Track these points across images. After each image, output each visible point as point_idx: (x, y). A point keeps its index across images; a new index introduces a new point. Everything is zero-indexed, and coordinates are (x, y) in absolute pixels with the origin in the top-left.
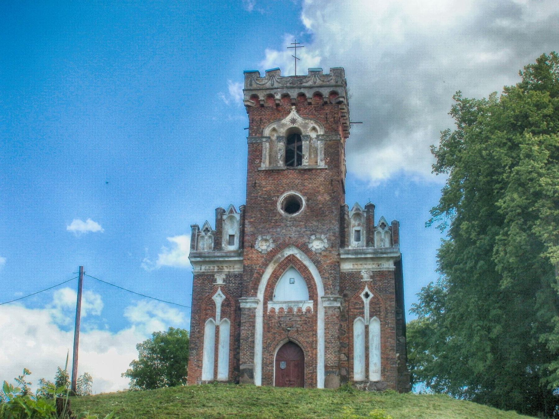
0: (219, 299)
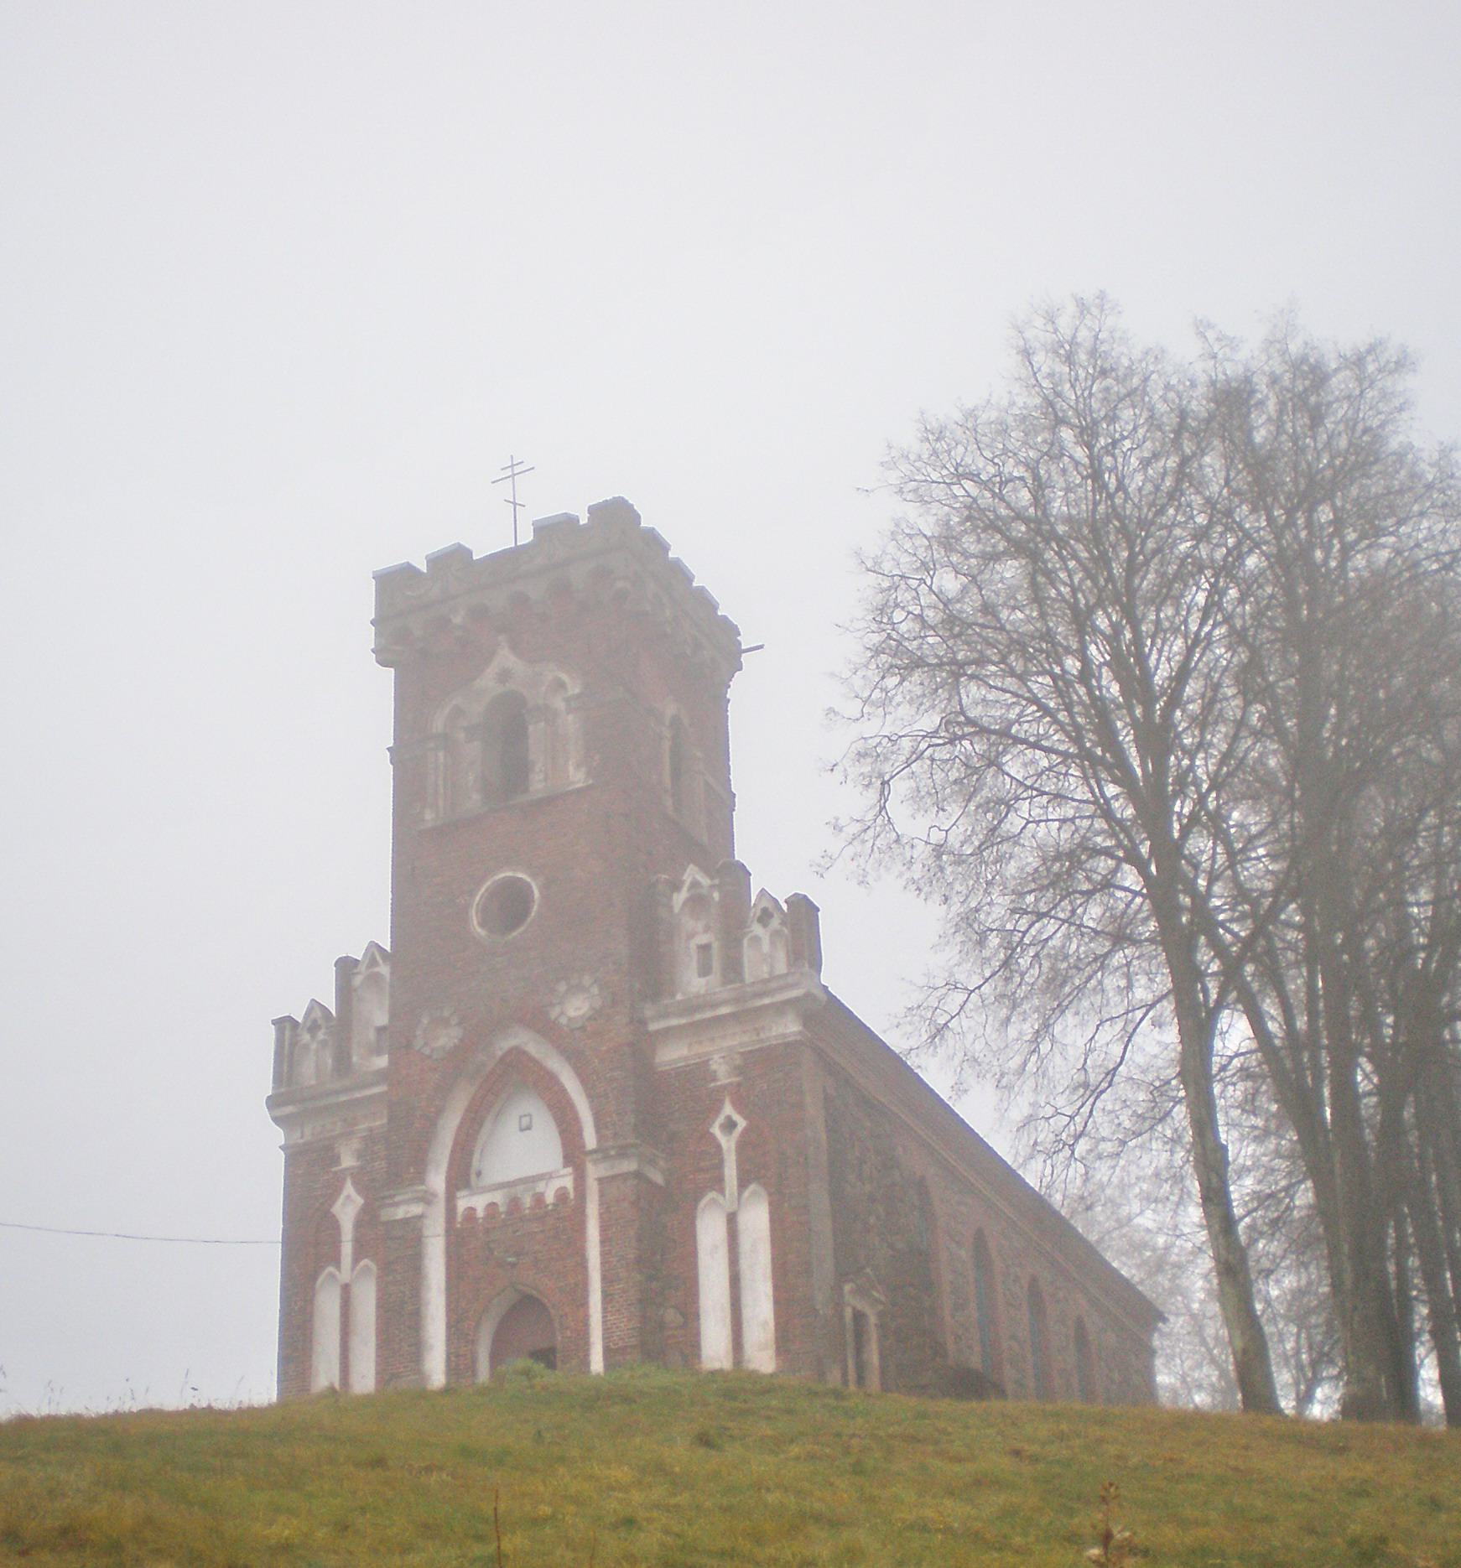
0: (348, 1208)
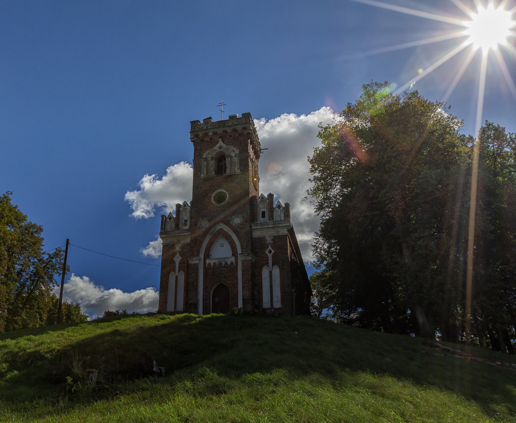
0: (178, 259)
